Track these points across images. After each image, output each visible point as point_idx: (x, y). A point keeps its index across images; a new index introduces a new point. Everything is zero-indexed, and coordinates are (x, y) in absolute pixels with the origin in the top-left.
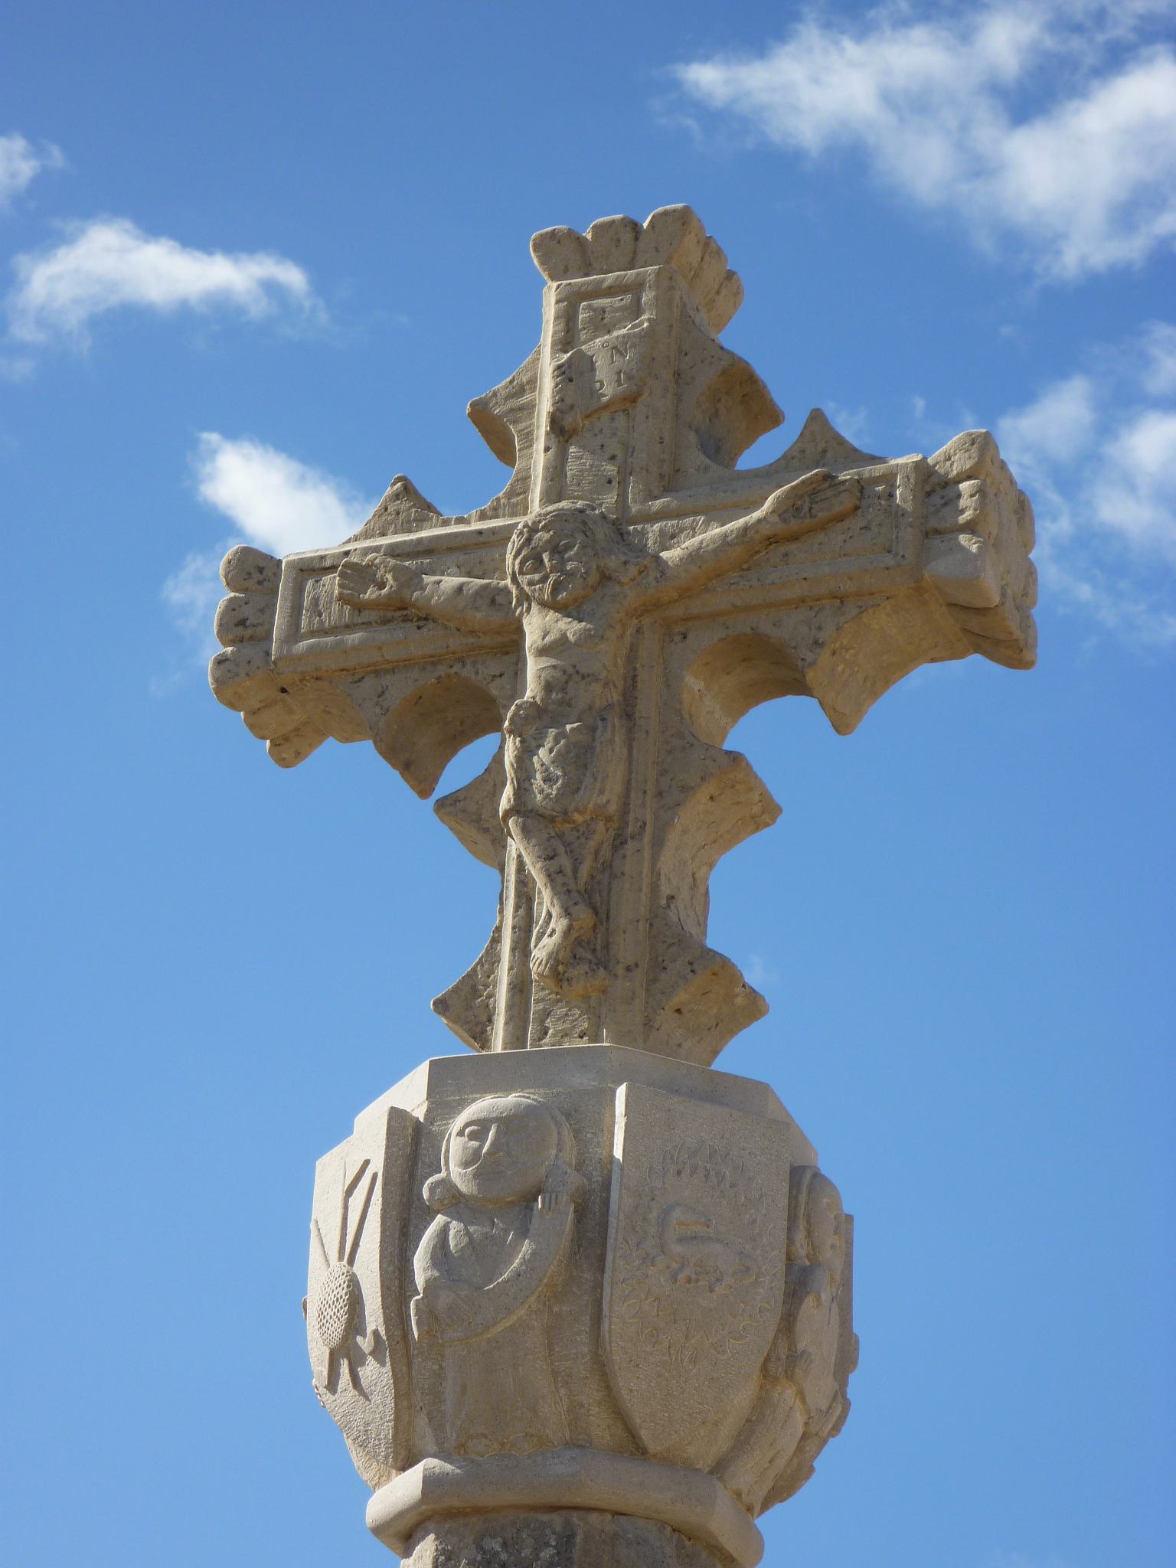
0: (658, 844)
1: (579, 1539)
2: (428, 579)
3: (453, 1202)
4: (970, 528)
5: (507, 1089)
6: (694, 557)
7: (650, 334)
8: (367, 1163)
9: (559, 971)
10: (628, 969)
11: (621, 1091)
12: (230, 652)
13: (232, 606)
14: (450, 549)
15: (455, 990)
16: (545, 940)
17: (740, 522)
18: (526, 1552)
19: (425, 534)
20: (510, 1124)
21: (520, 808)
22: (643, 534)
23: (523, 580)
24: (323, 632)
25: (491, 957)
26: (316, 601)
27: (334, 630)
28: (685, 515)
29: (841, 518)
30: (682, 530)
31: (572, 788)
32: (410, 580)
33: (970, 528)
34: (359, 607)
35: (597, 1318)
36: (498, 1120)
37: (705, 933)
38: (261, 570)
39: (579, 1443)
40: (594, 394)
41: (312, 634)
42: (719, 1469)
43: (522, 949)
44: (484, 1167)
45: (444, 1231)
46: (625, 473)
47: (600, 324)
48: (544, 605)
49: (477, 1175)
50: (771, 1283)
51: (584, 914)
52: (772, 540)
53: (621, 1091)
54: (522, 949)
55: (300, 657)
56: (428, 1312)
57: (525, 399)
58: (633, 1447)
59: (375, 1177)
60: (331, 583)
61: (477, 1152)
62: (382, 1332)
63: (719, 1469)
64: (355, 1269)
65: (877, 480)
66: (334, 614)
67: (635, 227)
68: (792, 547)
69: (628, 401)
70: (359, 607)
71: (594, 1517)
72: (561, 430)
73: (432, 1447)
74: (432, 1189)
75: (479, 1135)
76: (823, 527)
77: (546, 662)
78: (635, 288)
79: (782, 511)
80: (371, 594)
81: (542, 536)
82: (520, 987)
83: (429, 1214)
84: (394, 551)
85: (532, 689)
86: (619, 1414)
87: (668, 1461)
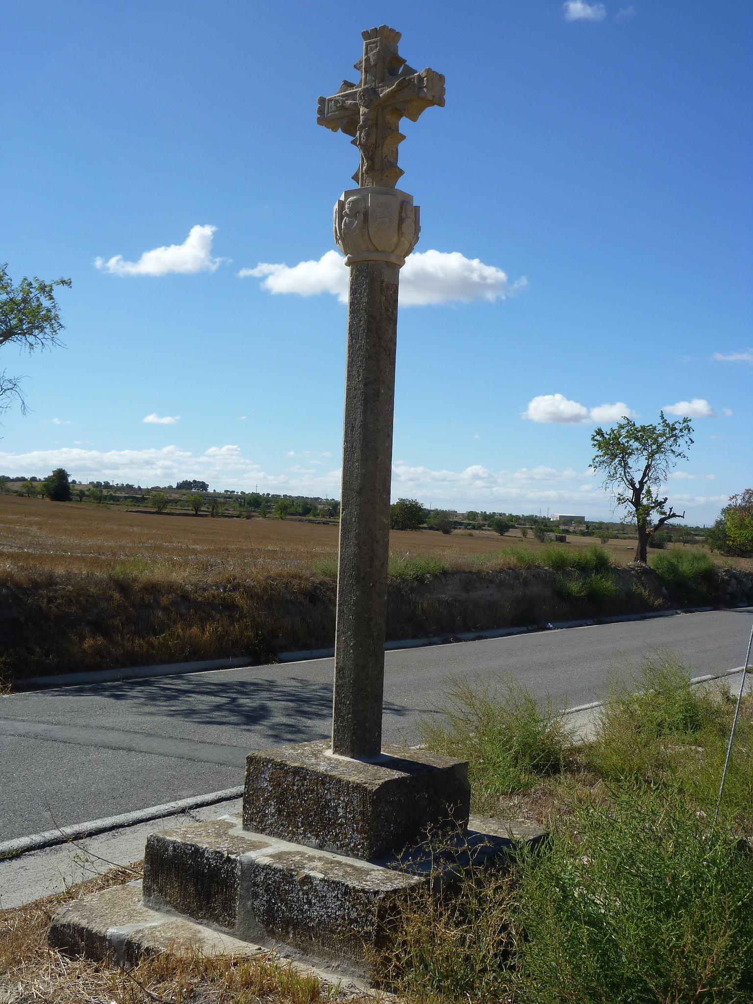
0: (382, 147)
1: (369, 265)
2: (346, 101)
3: (347, 215)
4: (425, 87)
7: (379, 52)
10: (378, 170)
12: (366, 110)
14: (350, 95)
15: (354, 175)
17: (347, 92)
18: (363, 268)
19: (347, 92)
20: (353, 202)
22: (378, 90)
23: (360, 101)
28: (384, 87)
29: (406, 86)
30: (384, 89)
31: (367, 140)
32: (343, 102)
33: (425, 87)
35: (368, 232)
36: (352, 202)
37: (397, 160)
38: (323, 100)
39: (368, 251)
40: (370, 64)
42: (393, 252)
43: (362, 168)
44: (350, 209)
45: (346, 219)
46: (375, 79)
47: (371, 50)
48: (363, 106)
50: (396, 221)
52: (396, 91)
54: (362, 168)
55: (330, 117)
56: (344, 233)
58: (377, 250)
63: (393, 252)
65: (412, 79)
66: (334, 108)
67: (376, 29)
68: (400, 92)
69: (375, 65)
70: (337, 107)
75: (349, 204)
77: (363, 117)
79: (398, 85)
80: (338, 105)
82: (362, 175)
84: (343, 96)
87: (383, 252)
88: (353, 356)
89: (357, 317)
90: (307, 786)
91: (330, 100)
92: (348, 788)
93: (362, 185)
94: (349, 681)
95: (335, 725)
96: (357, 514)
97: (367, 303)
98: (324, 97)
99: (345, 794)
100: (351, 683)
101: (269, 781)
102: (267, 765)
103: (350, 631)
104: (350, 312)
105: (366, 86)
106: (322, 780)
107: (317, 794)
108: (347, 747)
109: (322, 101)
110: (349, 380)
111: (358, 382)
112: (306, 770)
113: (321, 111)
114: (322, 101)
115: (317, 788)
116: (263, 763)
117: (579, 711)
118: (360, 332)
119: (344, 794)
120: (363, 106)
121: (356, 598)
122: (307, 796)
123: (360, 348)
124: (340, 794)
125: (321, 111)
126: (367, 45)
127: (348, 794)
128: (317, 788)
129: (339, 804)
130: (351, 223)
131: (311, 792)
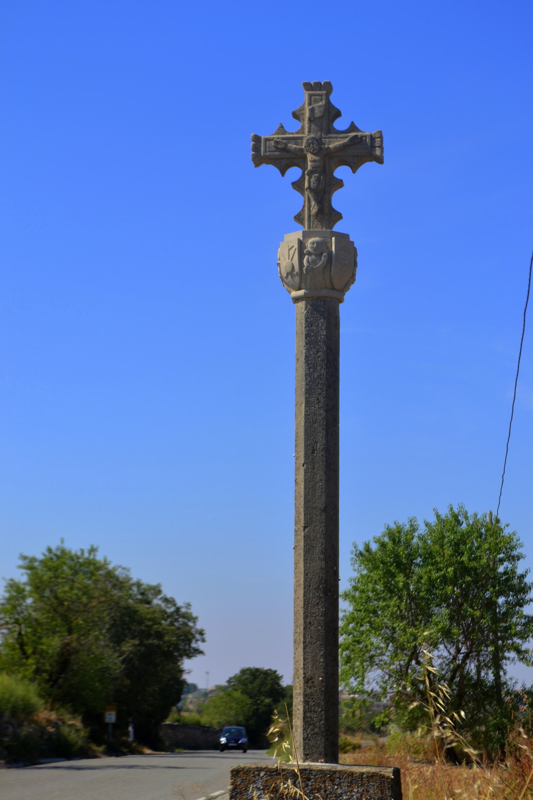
3: (309, 254)
5: (315, 237)
6: (335, 148)
8: (293, 246)
9: (317, 214)
11: (333, 239)
13: (254, 145)
16: (314, 210)
21: (309, 188)
24: (271, 151)
25: (303, 210)
26: (269, 146)
27: (273, 151)
34: (277, 148)
41: (269, 152)
45: (308, 259)
47: (316, 101)
49: (314, 250)
51: (320, 206)
52: (348, 145)
53: (333, 239)
56: (306, 270)
57: (302, 112)
58: (333, 289)
59: (296, 249)
60: (272, 143)
61: (313, 247)
62: (298, 272)
64: (293, 262)
66: (273, 149)
67: (320, 83)
69: (321, 117)
70: (277, 148)
71: (328, 298)
72: (310, 120)
73: (304, 287)
74: (306, 251)
76: (355, 144)
77: (312, 163)
78: (321, 95)
81: (310, 141)
82: (309, 216)
83: (305, 255)
85: (309, 168)
86: (331, 283)
88: (311, 384)
89: (314, 347)
90: (312, 786)
91: (267, 140)
92: (362, 778)
93: (309, 227)
94: (320, 689)
95: (305, 734)
96: (322, 531)
97: (326, 336)
98: (259, 135)
99: (360, 785)
100: (323, 691)
101: (263, 789)
102: (259, 775)
103: (319, 641)
104: (306, 343)
105: (312, 135)
106: (330, 777)
107: (325, 791)
108: (320, 753)
109: (257, 139)
110: (307, 406)
111: (318, 408)
112: (310, 771)
113: (256, 148)
114: (257, 139)
115: (325, 786)
116: (253, 773)
117: (131, 767)
118: (319, 362)
119: (358, 785)
120: (312, 153)
121: (325, 610)
122: (313, 796)
123: (319, 377)
124: (353, 787)
125: (256, 148)
126: (310, 96)
127: (362, 785)
128: (325, 786)
129: (353, 796)
130: (314, 262)
131: (318, 790)
